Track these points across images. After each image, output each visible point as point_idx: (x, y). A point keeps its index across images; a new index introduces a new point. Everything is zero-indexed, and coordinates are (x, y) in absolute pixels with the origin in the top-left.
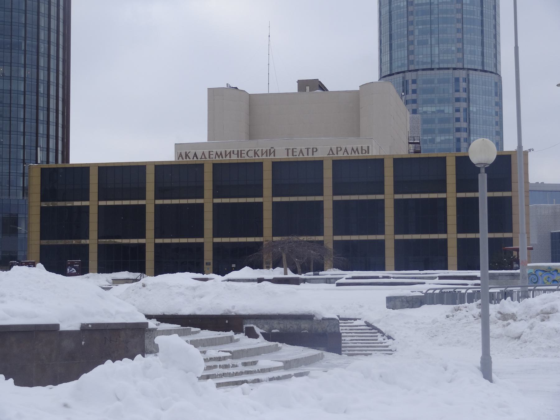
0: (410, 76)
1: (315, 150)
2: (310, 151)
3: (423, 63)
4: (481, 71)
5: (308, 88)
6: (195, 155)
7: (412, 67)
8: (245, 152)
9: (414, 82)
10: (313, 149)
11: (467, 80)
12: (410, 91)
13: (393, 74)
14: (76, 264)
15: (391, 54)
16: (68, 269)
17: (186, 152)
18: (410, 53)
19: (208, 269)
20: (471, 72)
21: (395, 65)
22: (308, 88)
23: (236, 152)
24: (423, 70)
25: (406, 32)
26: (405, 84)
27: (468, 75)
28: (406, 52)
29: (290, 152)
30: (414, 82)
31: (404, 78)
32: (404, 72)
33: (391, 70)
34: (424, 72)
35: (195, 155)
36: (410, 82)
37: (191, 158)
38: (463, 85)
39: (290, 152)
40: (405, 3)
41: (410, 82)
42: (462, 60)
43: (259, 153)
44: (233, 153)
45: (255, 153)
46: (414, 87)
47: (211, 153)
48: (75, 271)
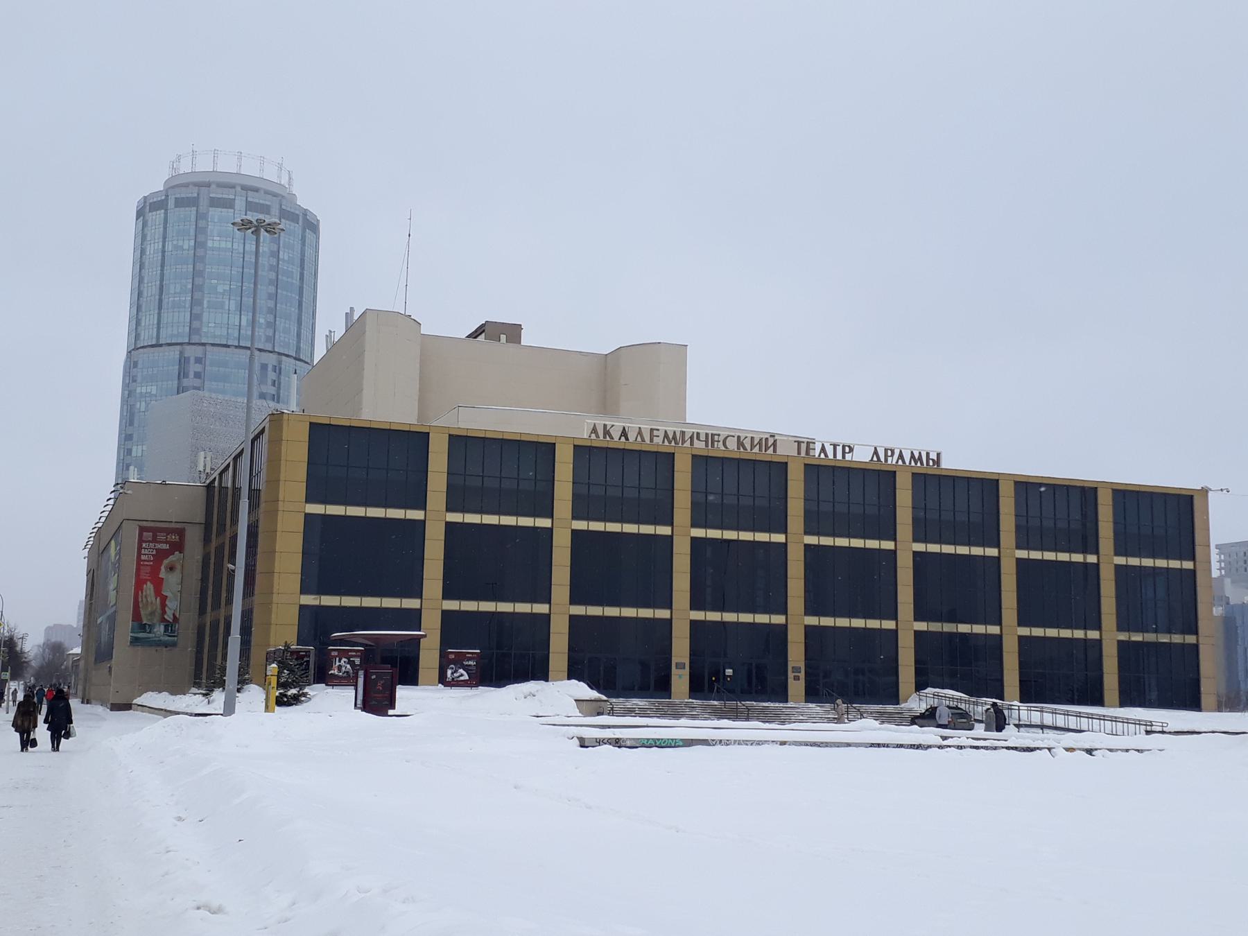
0: (191, 352)
1: (847, 449)
2: (839, 449)
3: (215, 336)
4: (296, 359)
5: (503, 337)
6: (624, 433)
7: (195, 339)
8: (721, 438)
9: (198, 360)
10: (844, 447)
11: (278, 370)
12: (191, 375)
13: (161, 345)
14: (469, 659)
15: (159, 314)
16: (449, 672)
17: (605, 426)
18: (195, 317)
19: (680, 676)
20: (284, 358)
21: (163, 333)
22: (503, 337)
23: (703, 437)
24: (213, 345)
25: (190, 286)
26: (183, 361)
27: (280, 362)
28: (188, 315)
29: (804, 447)
30: (198, 360)
31: (181, 353)
32: (181, 344)
33: (158, 337)
34: (216, 349)
35: (624, 433)
36: (192, 360)
37: (616, 439)
38: (272, 376)
39: (804, 447)
40: (192, 243)
41: (192, 360)
42: (271, 340)
43: (747, 444)
44: (698, 438)
45: (740, 443)
46: (198, 368)
47: (655, 433)
48: (466, 677)
